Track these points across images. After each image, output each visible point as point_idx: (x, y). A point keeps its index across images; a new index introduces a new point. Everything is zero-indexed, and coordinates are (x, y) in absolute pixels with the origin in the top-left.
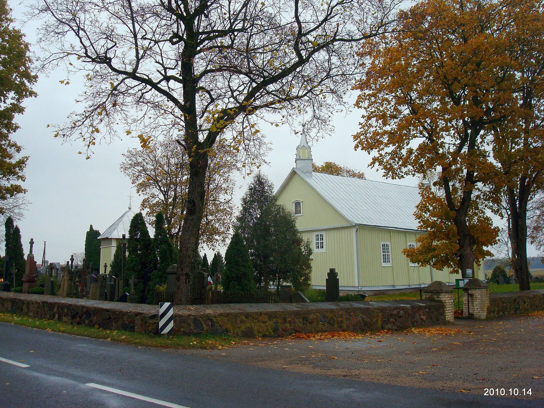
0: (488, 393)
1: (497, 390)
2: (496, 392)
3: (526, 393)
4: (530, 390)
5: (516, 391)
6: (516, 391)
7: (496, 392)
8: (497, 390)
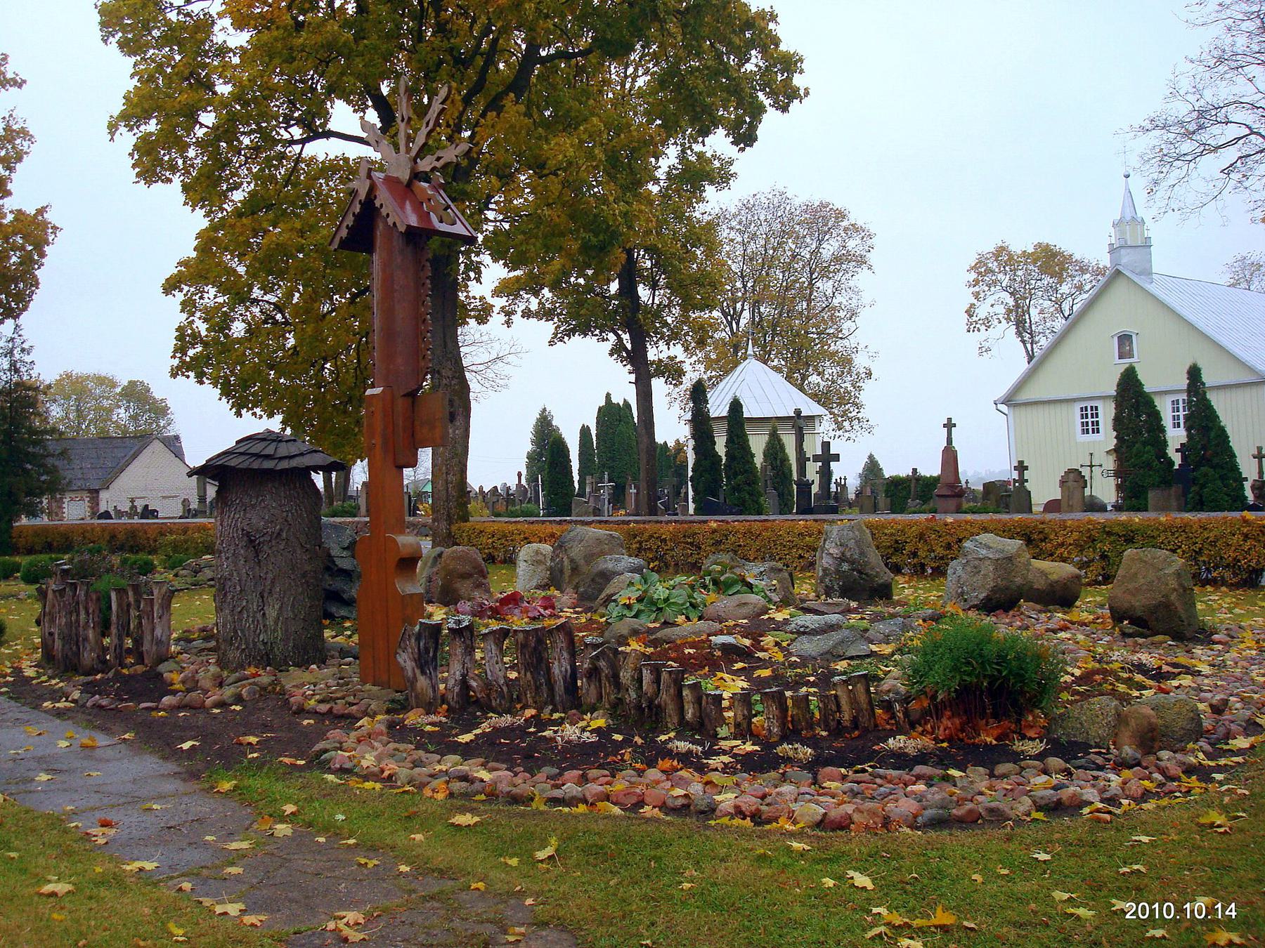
0: (1135, 913)
1: (1156, 905)
2: (1152, 911)
3: (1223, 912)
4: (1233, 905)
5: (1169, 908)
6: (1169, 908)
7: (1152, 911)
8: (1156, 905)
